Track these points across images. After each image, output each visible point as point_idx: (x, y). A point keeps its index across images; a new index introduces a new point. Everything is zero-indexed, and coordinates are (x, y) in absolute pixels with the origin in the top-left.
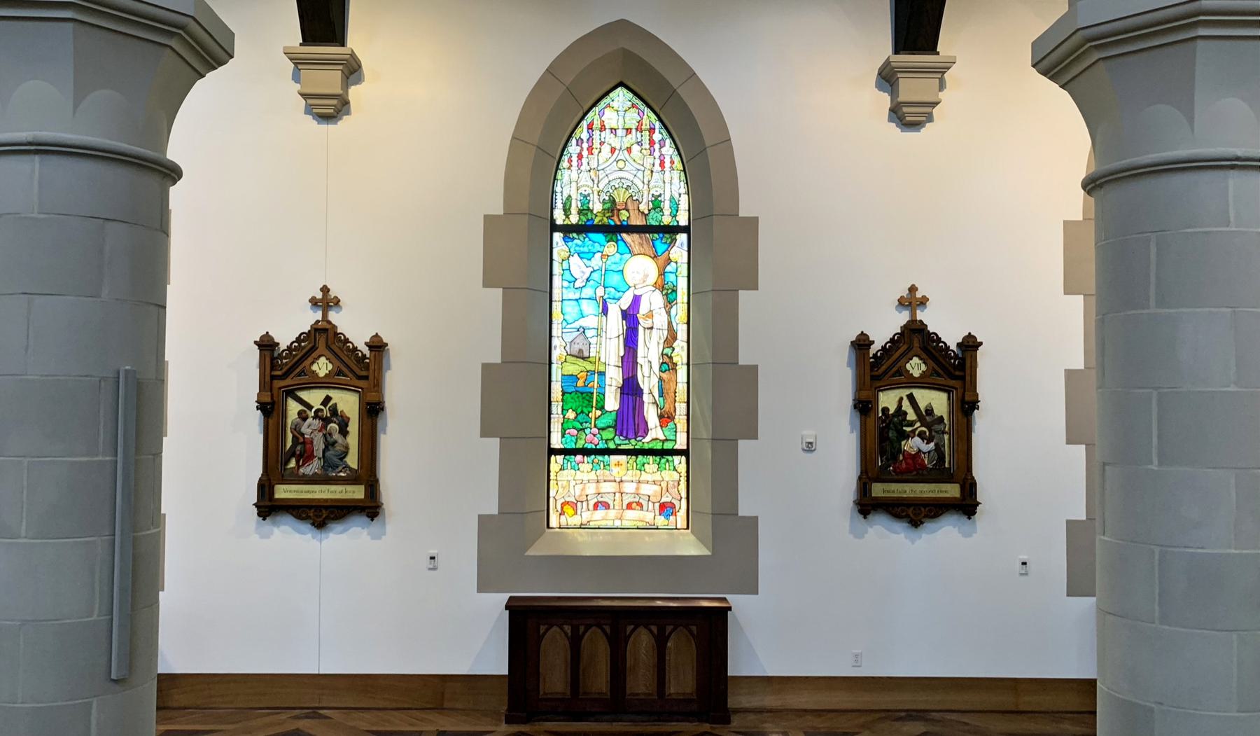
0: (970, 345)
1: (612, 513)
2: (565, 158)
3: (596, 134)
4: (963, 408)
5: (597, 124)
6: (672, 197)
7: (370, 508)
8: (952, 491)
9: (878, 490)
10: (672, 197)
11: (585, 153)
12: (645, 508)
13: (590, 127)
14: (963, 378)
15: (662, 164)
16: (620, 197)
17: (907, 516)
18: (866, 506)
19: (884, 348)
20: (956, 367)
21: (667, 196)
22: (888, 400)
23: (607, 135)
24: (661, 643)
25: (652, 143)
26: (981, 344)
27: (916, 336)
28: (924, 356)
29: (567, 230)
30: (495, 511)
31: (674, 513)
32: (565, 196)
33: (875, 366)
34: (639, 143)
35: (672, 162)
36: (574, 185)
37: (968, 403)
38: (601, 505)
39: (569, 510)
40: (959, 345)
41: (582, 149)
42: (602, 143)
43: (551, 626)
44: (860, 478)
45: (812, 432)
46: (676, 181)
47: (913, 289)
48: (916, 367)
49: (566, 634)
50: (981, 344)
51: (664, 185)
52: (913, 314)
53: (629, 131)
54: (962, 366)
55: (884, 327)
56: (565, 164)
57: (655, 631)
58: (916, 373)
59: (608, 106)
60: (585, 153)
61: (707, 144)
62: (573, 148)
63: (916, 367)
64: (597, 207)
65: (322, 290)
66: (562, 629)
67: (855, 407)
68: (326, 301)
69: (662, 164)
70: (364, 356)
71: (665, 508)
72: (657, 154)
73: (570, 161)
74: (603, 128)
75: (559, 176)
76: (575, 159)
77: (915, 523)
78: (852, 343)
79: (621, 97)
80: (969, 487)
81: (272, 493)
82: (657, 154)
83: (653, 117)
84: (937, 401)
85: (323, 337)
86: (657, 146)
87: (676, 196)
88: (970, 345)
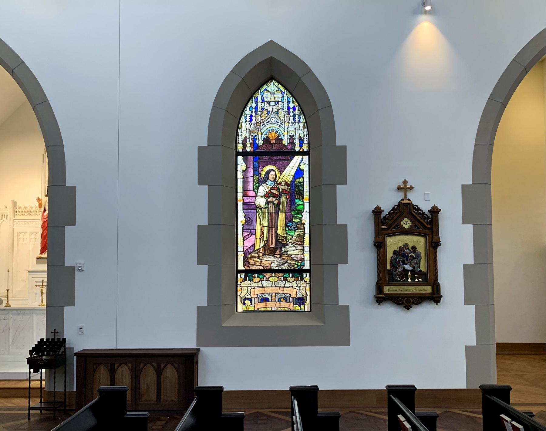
0: (435, 211)
1: (269, 304)
2: (243, 117)
3: (259, 105)
4: (432, 245)
5: (260, 100)
6: (300, 137)
7: (435, 297)
8: (428, 289)
9: (387, 289)
10: (300, 137)
11: (254, 114)
12: (270, 300)
13: (256, 102)
14: (431, 229)
15: (294, 120)
16: (272, 137)
17: (403, 304)
18: (381, 298)
19: (389, 213)
20: (427, 224)
21: (297, 136)
22: (394, 243)
23: (267, 106)
24: (159, 372)
25: (289, 108)
26: (440, 210)
27: (405, 209)
28: (410, 216)
29: (245, 154)
30: (206, 304)
31: (303, 303)
32: (244, 136)
33: (385, 224)
34: (283, 109)
35: (299, 118)
36: (247, 131)
37: (434, 242)
38: (265, 300)
39: (247, 302)
40: (429, 211)
41: (252, 112)
42: (263, 109)
43: (121, 364)
44: (377, 283)
45: (83, 262)
46: (301, 128)
47: (405, 182)
48: (406, 223)
49: (154, 368)
50: (440, 210)
51: (293, 130)
52: (405, 195)
53: (277, 102)
54: (431, 223)
55: (388, 202)
56: (243, 120)
57: (156, 367)
58: (406, 227)
59: (266, 90)
60: (254, 114)
61: (319, 107)
62: (247, 112)
63: (406, 223)
64: (260, 142)
65: (411, 186)
66: (127, 366)
67: (375, 245)
68: (405, 188)
69: (294, 120)
70: (428, 217)
71: (300, 301)
72: (291, 114)
73: (246, 118)
74: (263, 101)
75: (240, 126)
76: (248, 117)
77: (408, 308)
78: (373, 212)
79: (273, 86)
80: (436, 287)
81: (433, 289)
82: (291, 114)
83: (289, 95)
84: (419, 242)
85: (405, 209)
86: (291, 110)
87: (302, 136)
88: (435, 211)
